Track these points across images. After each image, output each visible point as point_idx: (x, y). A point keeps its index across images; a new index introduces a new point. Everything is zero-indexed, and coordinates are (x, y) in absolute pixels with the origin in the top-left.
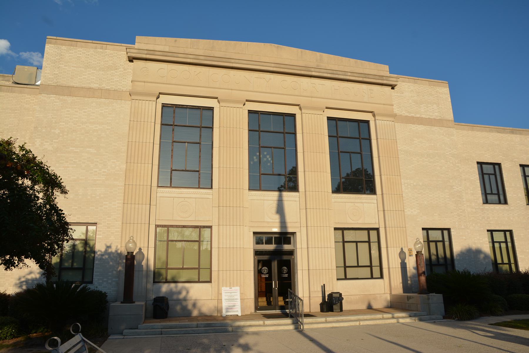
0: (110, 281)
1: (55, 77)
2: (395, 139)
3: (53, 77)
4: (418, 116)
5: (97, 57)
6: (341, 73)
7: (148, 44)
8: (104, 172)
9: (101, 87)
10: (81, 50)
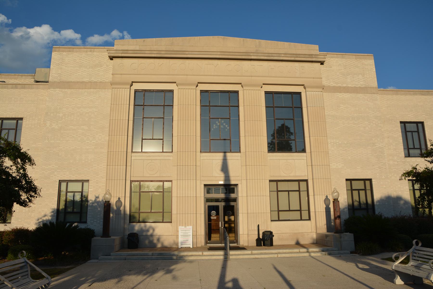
0: (98, 222)
3: (58, 76)
4: (345, 85)
6: (275, 55)
8: (93, 143)
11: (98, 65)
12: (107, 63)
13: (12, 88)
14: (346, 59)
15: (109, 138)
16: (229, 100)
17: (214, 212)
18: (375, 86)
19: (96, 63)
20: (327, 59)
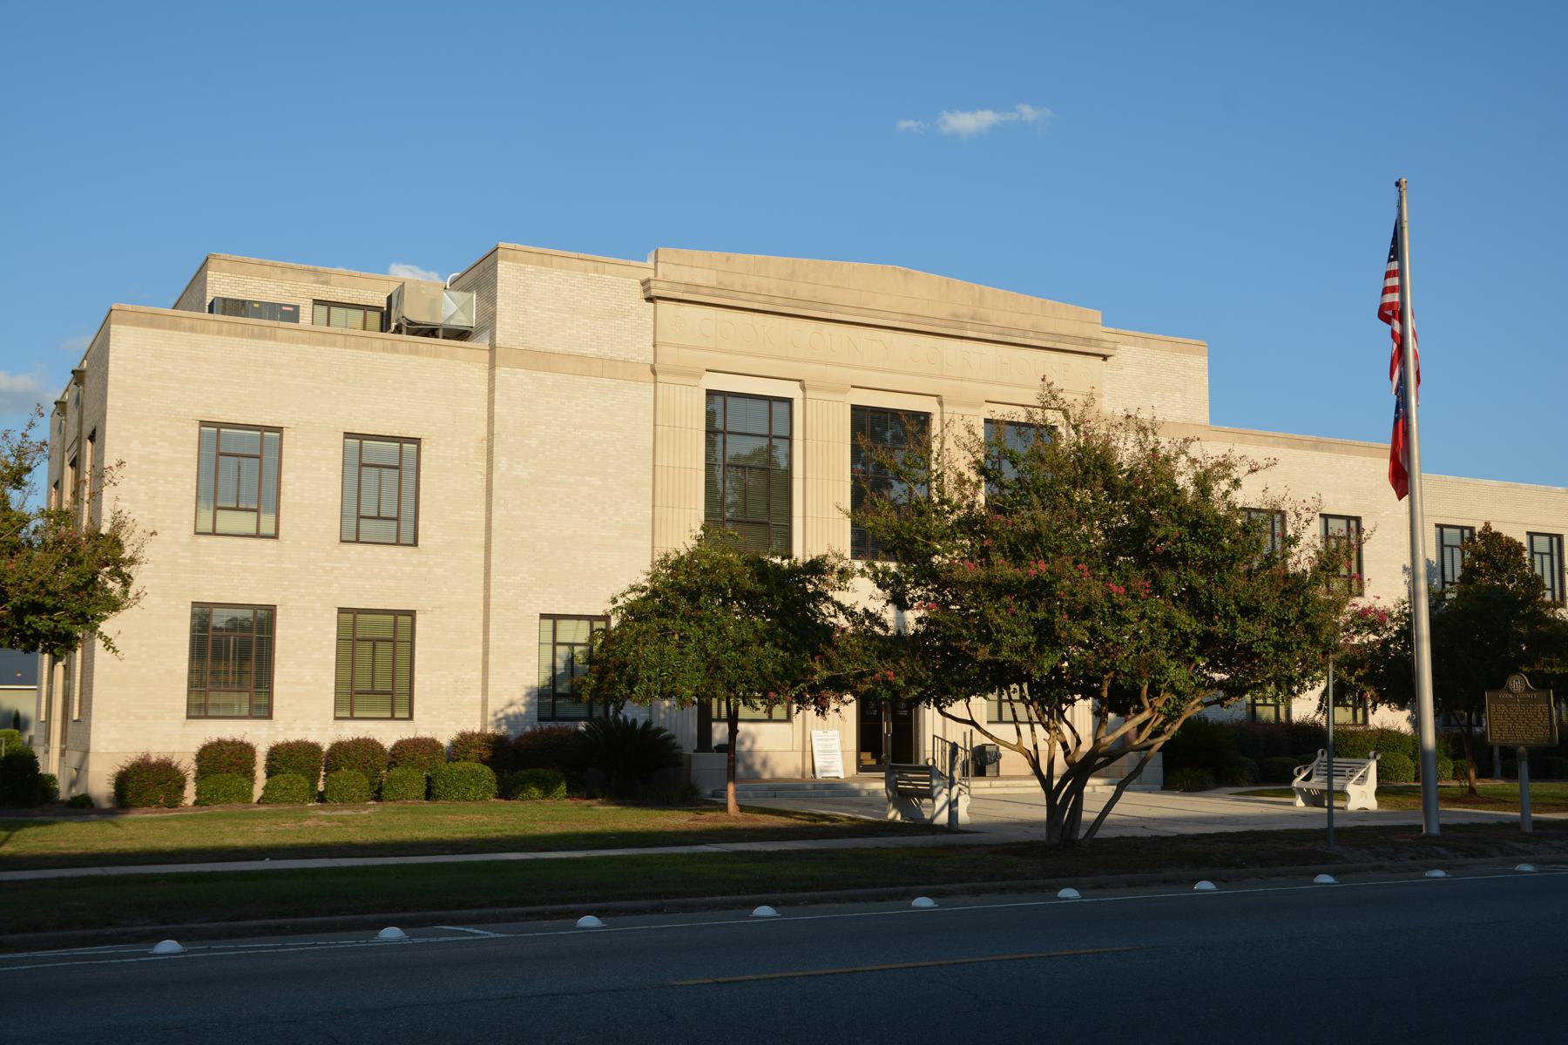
3: (517, 331)
6: (1017, 333)
13: (384, 350)
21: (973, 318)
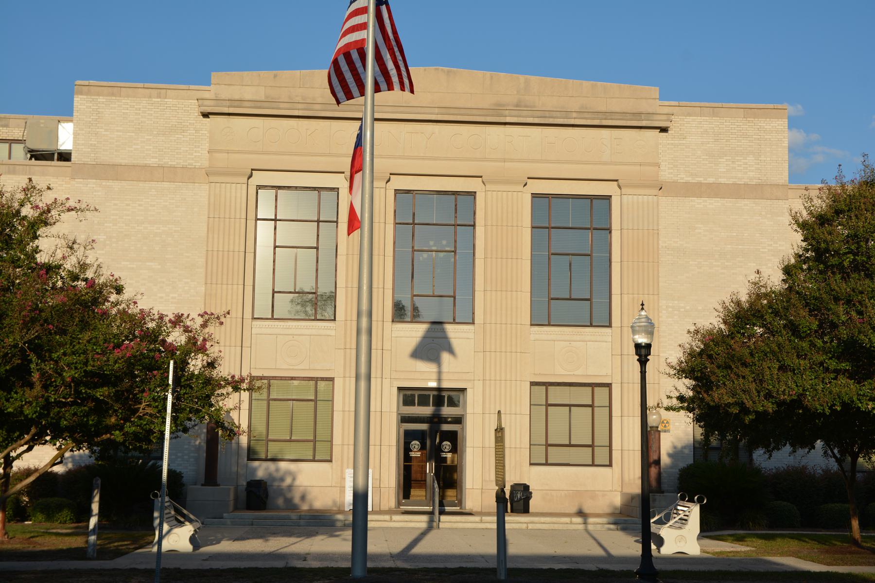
0: (186, 457)
1: (92, 150)
2: (655, 228)
3: (90, 150)
4: (711, 180)
5: (153, 112)
6: (558, 114)
7: (231, 85)
8: (173, 298)
9: (162, 163)
10: (128, 101)
11: (176, 128)
12: (195, 124)
14: (722, 119)
15: (205, 290)
16: (456, 212)
17: (415, 444)
18: (783, 181)
19: (171, 123)
20: (678, 120)
21: (517, 106)
